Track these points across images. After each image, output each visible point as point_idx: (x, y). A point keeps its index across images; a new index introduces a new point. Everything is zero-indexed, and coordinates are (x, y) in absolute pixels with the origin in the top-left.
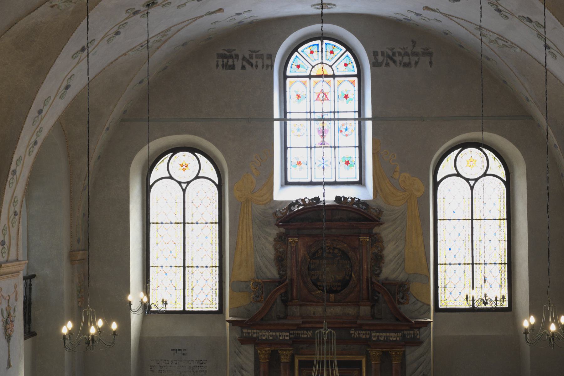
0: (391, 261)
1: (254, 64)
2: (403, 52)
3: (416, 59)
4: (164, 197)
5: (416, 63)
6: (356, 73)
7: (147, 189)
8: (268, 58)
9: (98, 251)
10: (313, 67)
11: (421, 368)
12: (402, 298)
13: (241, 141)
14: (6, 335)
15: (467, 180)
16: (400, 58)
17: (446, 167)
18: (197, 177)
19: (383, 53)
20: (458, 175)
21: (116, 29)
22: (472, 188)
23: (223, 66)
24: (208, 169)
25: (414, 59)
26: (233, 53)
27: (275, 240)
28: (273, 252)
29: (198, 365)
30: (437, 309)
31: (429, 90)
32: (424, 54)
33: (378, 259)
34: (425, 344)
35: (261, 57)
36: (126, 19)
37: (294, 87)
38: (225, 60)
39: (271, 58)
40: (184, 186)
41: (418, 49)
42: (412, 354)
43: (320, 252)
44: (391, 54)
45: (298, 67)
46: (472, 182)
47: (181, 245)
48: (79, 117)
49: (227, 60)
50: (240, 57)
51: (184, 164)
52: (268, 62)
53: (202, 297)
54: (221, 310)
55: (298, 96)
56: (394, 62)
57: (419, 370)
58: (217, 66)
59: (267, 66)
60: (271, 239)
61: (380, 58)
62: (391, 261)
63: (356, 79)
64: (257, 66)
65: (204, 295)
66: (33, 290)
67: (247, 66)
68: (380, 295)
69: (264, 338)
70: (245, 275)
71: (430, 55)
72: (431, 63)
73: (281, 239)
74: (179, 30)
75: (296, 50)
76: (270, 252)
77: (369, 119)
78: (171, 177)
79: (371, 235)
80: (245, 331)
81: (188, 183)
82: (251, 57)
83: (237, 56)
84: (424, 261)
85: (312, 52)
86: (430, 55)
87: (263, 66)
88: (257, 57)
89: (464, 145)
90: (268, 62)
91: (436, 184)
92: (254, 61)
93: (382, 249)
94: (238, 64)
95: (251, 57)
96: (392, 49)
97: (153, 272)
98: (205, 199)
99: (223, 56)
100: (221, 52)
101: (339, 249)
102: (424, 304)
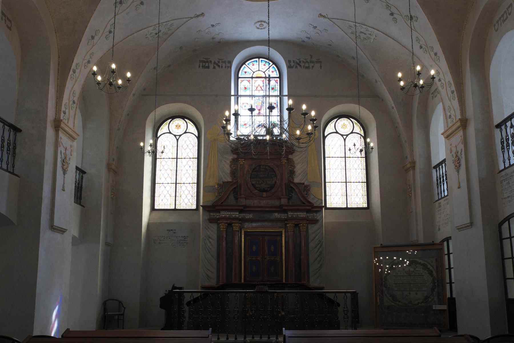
1: (221, 66)
2: (305, 61)
3: (312, 64)
4: (165, 142)
5: (313, 67)
6: (278, 76)
7: (156, 137)
8: (228, 63)
9: (126, 170)
10: (254, 72)
11: (317, 237)
12: (306, 194)
13: (209, 102)
14: (63, 168)
15: (342, 135)
16: (304, 64)
17: (330, 128)
18: (185, 132)
19: (294, 61)
20: (337, 132)
23: (203, 66)
24: (192, 128)
26: (209, 60)
27: (231, 162)
28: (229, 169)
30: (327, 209)
31: (322, 74)
33: (292, 173)
34: (320, 223)
35: (225, 62)
37: (242, 84)
38: (204, 64)
39: (230, 63)
40: (177, 137)
41: (314, 60)
42: (312, 229)
43: (257, 168)
44: (298, 61)
46: (344, 137)
47: (174, 172)
49: (205, 64)
50: (213, 62)
51: (178, 125)
53: (186, 201)
54: (197, 209)
55: (245, 88)
56: (300, 66)
57: (317, 238)
58: (199, 66)
59: (228, 67)
60: (229, 162)
61: (292, 64)
63: (278, 79)
64: (222, 67)
65: (188, 200)
66: (84, 181)
67: (216, 67)
68: (293, 194)
69: (223, 216)
70: (213, 182)
71: (321, 62)
72: (321, 67)
73: (234, 162)
74: (178, 28)
75: (244, 63)
76: (227, 169)
77: (286, 96)
78: (170, 133)
79: (288, 159)
80: (212, 214)
81: (180, 136)
82: (219, 62)
83: (211, 61)
84: (319, 175)
86: (321, 62)
87: (225, 67)
88: (222, 62)
89: (340, 116)
90: (229, 65)
91: (324, 137)
93: (294, 167)
94: (211, 66)
95: (219, 62)
98: (189, 145)
100: (202, 59)
101: (269, 166)
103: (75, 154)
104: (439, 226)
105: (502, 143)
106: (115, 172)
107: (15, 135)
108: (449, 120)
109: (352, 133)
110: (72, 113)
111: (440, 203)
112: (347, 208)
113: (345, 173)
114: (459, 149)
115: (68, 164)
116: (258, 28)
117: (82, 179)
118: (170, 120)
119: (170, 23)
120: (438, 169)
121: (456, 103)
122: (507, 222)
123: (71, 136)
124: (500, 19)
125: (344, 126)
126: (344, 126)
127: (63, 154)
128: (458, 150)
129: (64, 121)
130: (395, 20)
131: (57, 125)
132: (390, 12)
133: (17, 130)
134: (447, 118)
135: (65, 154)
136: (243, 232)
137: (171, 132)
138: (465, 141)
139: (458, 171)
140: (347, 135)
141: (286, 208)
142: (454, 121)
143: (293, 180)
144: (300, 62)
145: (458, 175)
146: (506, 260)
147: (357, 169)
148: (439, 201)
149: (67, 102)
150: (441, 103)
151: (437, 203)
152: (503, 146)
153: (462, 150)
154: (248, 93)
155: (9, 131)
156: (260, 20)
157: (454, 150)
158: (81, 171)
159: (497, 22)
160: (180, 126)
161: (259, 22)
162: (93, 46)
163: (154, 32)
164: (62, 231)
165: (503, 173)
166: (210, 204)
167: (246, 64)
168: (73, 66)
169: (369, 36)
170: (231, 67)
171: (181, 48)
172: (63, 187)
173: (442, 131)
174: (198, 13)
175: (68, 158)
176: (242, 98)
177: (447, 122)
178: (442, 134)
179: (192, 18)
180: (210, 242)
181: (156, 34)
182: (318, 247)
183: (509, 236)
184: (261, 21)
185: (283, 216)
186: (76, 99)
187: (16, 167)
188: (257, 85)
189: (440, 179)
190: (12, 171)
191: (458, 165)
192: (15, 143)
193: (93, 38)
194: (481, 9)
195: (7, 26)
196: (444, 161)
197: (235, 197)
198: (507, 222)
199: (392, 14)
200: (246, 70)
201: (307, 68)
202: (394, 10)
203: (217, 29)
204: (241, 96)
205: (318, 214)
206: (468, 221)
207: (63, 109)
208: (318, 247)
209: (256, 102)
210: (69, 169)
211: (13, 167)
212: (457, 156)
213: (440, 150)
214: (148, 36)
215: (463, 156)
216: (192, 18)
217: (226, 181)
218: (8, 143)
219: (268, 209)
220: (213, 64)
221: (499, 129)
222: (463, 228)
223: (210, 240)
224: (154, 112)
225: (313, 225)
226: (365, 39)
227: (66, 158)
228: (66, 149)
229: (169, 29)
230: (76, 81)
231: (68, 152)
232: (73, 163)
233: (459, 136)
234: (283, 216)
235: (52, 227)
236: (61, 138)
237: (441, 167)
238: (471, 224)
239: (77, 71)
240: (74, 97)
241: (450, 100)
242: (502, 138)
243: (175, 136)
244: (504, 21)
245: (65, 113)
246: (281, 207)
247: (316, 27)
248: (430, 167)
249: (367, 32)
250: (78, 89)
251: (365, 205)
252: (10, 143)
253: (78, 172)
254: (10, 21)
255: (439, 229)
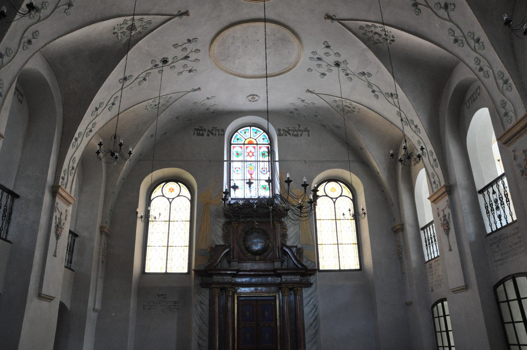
0: (292, 237)
3: (301, 133)
4: (158, 206)
5: (301, 135)
11: (312, 300)
13: (205, 171)
21: (143, 75)
22: (334, 203)
23: (197, 134)
24: (185, 191)
25: (299, 133)
27: (224, 225)
29: (173, 304)
32: (305, 131)
33: (284, 236)
34: (314, 286)
35: (218, 130)
36: (150, 69)
37: (235, 150)
39: (224, 131)
40: (170, 201)
44: (287, 130)
45: (238, 139)
46: (334, 200)
47: (168, 237)
48: (112, 148)
49: (200, 132)
50: (207, 130)
52: (221, 133)
54: (189, 272)
57: (311, 302)
58: (194, 134)
59: (221, 135)
60: (221, 225)
61: (282, 132)
62: (292, 237)
64: (215, 135)
65: (179, 264)
67: (210, 135)
71: (308, 131)
72: (309, 135)
73: (227, 225)
75: (236, 131)
77: (277, 161)
82: (213, 130)
84: (311, 237)
85: (245, 133)
88: (216, 130)
90: (221, 133)
92: (214, 132)
94: (205, 134)
96: (288, 128)
97: (148, 249)
99: (198, 130)
102: (312, 262)
103: (69, 218)
104: (432, 287)
105: (486, 207)
106: (107, 235)
107: (13, 201)
108: (434, 186)
109: (341, 196)
110: (70, 178)
111: (431, 264)
112: (340, 271)
113: (337, 239)
114: (446, 213)
115: (62, 229)
116: (250, 101)
117: (74, 242)
118: (163, 184)
119: (169, 96)
120: (425, 230)
121: (439, 170)
122: (502, 285)
123: (67, 201)
124: (470, 98)
125: (333, 190)
126: (333, 190)
127: (57, 220)
128: (445, 213)
129: (62, 187)
130: (377, 97)
131: (55, 191)
132: (371, 90)
133: (14, 196)
134: (431, 183)
135: (60, 219)
136: (236, 296)
137: (165, 195)
138: (452, 205)
139: (448, 234)
140: (336, 198)
141: (280, 272)
142: (439, 187)
143: (286, 242)
144: (289, 130)
145: (448, 237)
146: (506, 325)
147: (348, 229)
148: (430, 262)
149: (67, 168)
150: (424, 169)
151: (428, 264)
152: (487, 210)
153: (449, 214)
154: (240, 158)
155: (7, 197)
156: (252, 94)
157: (442, 214)
158: (73, 234)
159: (468, 101)
160: (173, 190)
161: (251, 95)
162: (97, 116)
163: (154, 104)
164: (50, 299)
165: (492, 236)
166: (202, 268)
167: (239, 131)
168: (76, 135)
169: (353, 109)
170: (224, 135)
171: (177, 118)
172: (55, 252)
173: (428, 196)
174: (195, 88)
175: (62, 222)
176: (234, 163)
177: (432, 187)
178: (429, 198)
179: (189, 92)
180: (202, 308)
181: (155, 105)
182: (313, 312)
183: (507, 303)
184: (254, 95)
185: (278, 280)
186: (75, 165)
187: (9, 233)
188: (248, 150)
189: (429, 240)
190: (4, 237)
191: (446, 228)
192: (11, 209)
193: (97, 109)
194: (453, 90)
195: (19, 100)
196: (431, 223)
197: (227, 261)
198: (502, 285)
199: (373, 91)
200: (238, 137)
201: (297, 136)
202: (375, 88)
203: (211, 102)
204: (233, 161)
205: (312, 277)
206: (462, 283)
207: (62, 175)
208: (313, 312)
209: (249, 171)
210: (62, 234)
211: (7, 233)
212: (445, 220)
213: (426, 213)
214: (148, 107)
215: (451, 219)
216: (189, 92)
217: (219, 244)
218: (4, 209)
219: (261, 273)
220: (206, 132)
221: (482, 195)
222: (458, 290)
223: (202, 306)
224: (151, 174)
225: (307, 289)
226: (349, 112)
227: (60, 223)
228: (61, 214)
229: (168, 102)
230: (77, 149)
231: (63, 217)
232: (66, 228)
233: (444, 202)
234: (278, 280)
235: (40, 296)
236: (57, 204)
237: (428, 228)
238: (466, 287)
239: (79, 140)
240: (74, 163)
241: (433, 167)
242: (486, 203)
243: (168, 199)
244: (474, 100)
245: (63, 179)
246: (275, 270)
247: (304, 100)
248: (418, 229)
249: (351, 106)
250: (78, 155)
251: (358, 267)
252: (6, 209)
253: (71, 235)
254: (22, 96)
255: (432, 290)
